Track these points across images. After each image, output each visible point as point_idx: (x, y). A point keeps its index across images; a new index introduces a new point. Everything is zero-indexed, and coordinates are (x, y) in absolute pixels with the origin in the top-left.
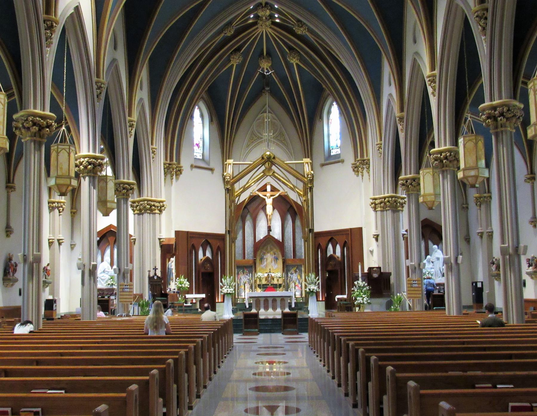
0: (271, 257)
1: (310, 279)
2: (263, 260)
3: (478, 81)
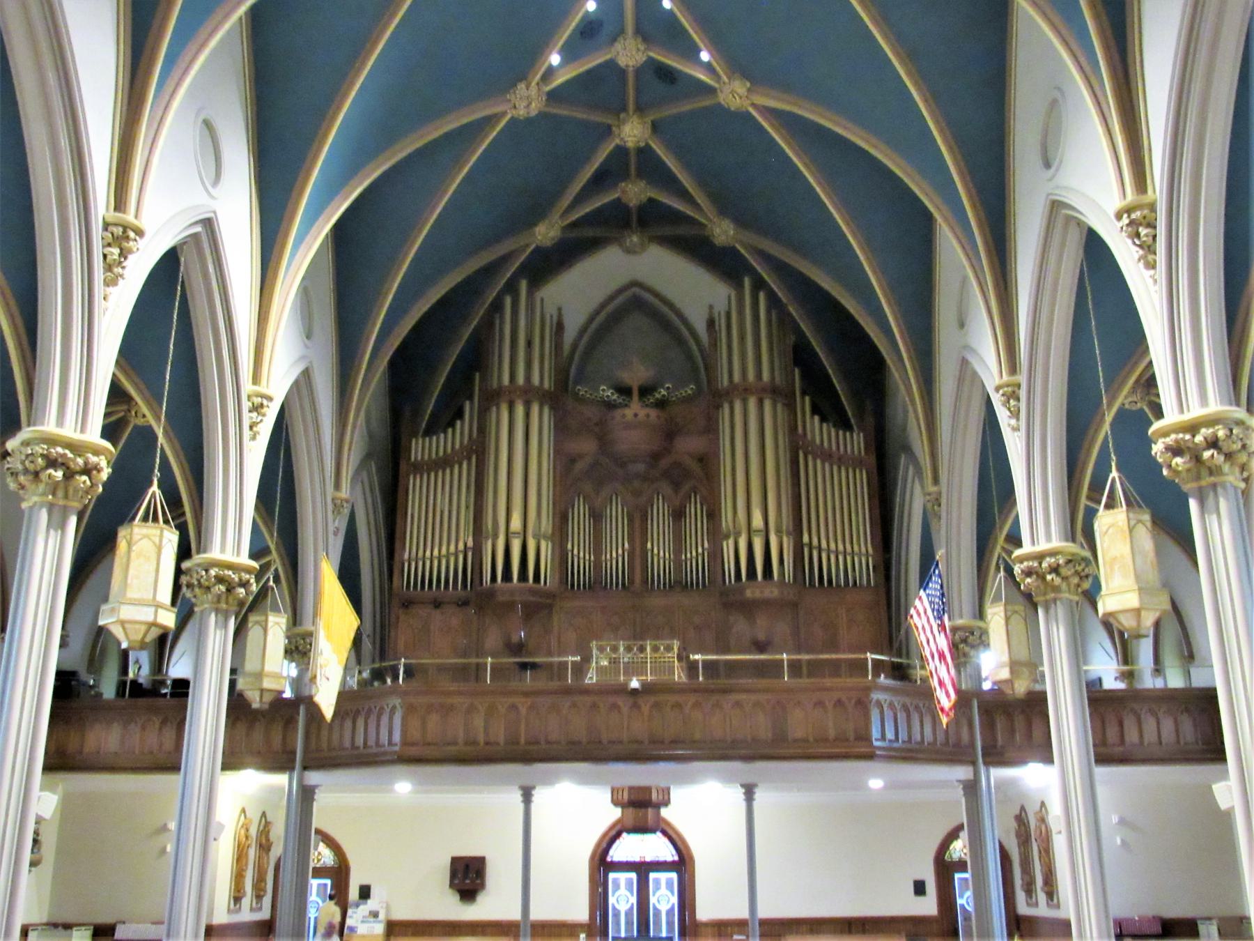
3: (1010, 511)
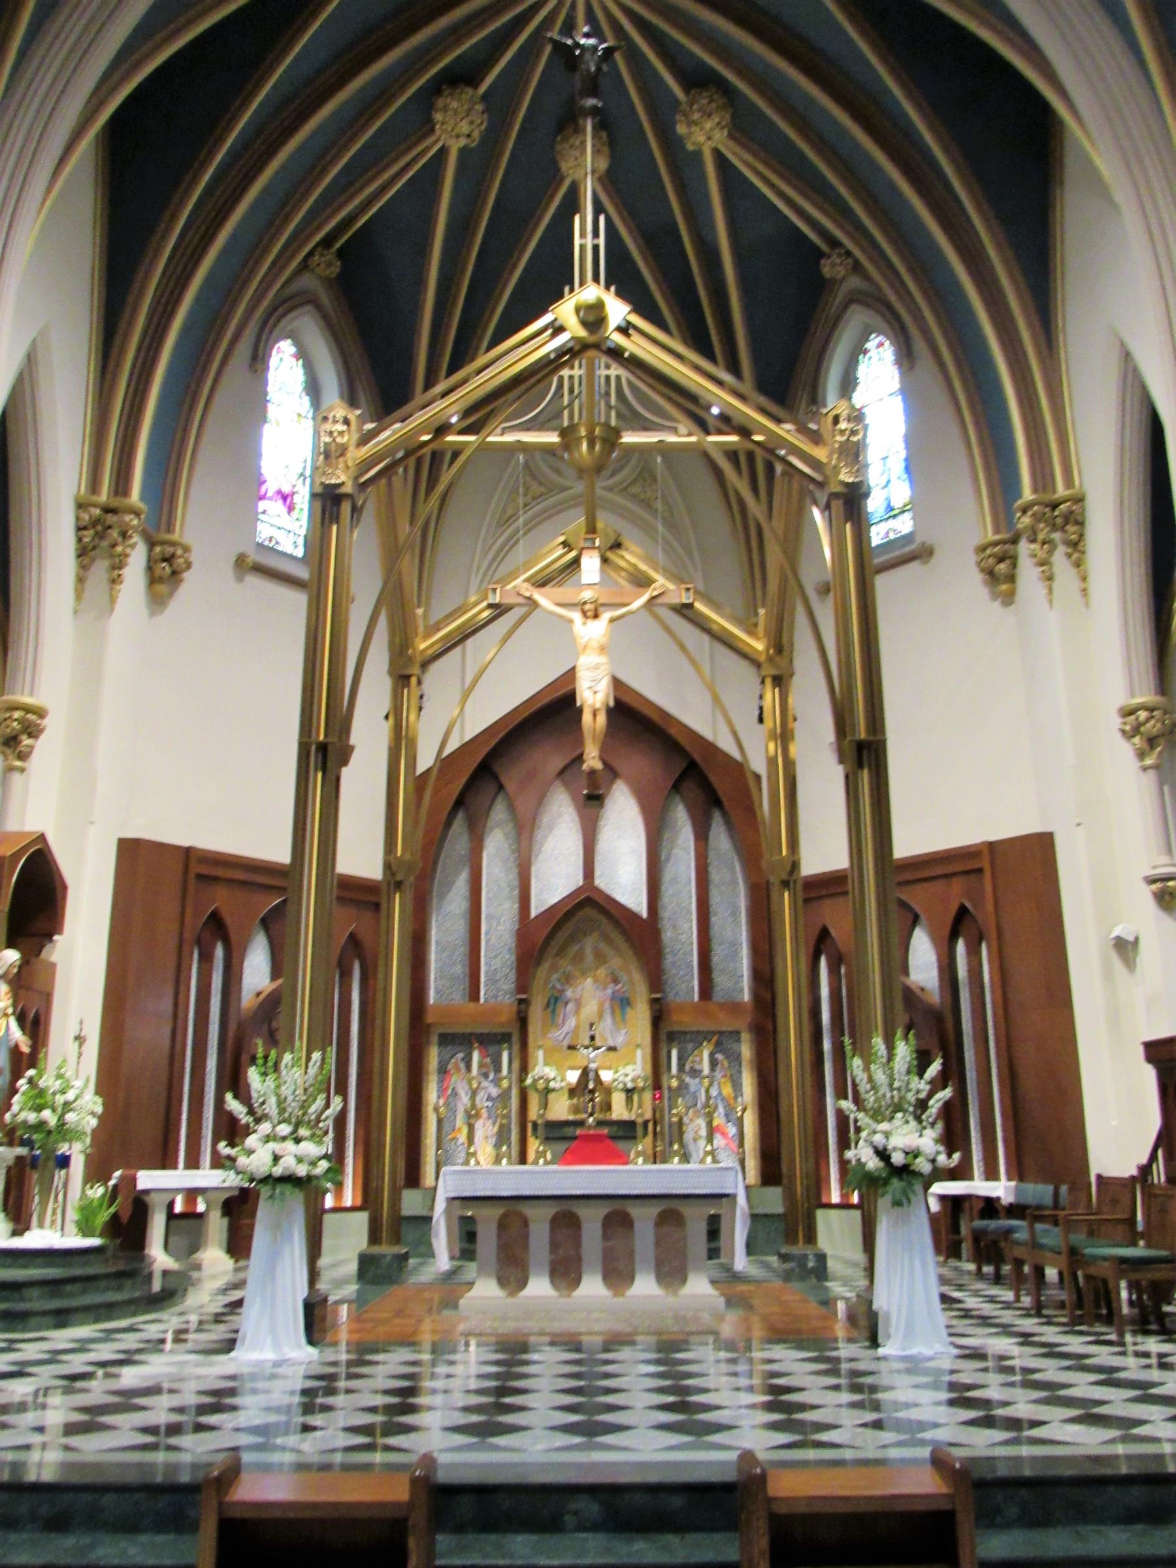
0: (599, 994)
1: (880, 1076)
2: (560, 1005)
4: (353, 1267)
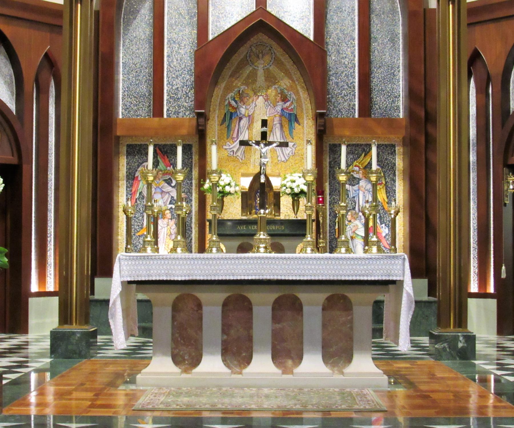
2: (235, 121)
4: (47, 344)
